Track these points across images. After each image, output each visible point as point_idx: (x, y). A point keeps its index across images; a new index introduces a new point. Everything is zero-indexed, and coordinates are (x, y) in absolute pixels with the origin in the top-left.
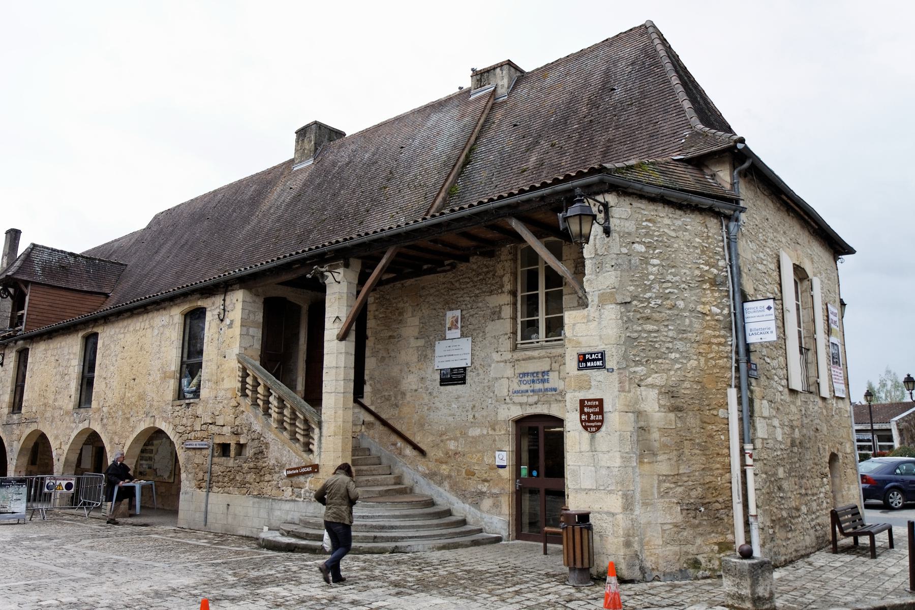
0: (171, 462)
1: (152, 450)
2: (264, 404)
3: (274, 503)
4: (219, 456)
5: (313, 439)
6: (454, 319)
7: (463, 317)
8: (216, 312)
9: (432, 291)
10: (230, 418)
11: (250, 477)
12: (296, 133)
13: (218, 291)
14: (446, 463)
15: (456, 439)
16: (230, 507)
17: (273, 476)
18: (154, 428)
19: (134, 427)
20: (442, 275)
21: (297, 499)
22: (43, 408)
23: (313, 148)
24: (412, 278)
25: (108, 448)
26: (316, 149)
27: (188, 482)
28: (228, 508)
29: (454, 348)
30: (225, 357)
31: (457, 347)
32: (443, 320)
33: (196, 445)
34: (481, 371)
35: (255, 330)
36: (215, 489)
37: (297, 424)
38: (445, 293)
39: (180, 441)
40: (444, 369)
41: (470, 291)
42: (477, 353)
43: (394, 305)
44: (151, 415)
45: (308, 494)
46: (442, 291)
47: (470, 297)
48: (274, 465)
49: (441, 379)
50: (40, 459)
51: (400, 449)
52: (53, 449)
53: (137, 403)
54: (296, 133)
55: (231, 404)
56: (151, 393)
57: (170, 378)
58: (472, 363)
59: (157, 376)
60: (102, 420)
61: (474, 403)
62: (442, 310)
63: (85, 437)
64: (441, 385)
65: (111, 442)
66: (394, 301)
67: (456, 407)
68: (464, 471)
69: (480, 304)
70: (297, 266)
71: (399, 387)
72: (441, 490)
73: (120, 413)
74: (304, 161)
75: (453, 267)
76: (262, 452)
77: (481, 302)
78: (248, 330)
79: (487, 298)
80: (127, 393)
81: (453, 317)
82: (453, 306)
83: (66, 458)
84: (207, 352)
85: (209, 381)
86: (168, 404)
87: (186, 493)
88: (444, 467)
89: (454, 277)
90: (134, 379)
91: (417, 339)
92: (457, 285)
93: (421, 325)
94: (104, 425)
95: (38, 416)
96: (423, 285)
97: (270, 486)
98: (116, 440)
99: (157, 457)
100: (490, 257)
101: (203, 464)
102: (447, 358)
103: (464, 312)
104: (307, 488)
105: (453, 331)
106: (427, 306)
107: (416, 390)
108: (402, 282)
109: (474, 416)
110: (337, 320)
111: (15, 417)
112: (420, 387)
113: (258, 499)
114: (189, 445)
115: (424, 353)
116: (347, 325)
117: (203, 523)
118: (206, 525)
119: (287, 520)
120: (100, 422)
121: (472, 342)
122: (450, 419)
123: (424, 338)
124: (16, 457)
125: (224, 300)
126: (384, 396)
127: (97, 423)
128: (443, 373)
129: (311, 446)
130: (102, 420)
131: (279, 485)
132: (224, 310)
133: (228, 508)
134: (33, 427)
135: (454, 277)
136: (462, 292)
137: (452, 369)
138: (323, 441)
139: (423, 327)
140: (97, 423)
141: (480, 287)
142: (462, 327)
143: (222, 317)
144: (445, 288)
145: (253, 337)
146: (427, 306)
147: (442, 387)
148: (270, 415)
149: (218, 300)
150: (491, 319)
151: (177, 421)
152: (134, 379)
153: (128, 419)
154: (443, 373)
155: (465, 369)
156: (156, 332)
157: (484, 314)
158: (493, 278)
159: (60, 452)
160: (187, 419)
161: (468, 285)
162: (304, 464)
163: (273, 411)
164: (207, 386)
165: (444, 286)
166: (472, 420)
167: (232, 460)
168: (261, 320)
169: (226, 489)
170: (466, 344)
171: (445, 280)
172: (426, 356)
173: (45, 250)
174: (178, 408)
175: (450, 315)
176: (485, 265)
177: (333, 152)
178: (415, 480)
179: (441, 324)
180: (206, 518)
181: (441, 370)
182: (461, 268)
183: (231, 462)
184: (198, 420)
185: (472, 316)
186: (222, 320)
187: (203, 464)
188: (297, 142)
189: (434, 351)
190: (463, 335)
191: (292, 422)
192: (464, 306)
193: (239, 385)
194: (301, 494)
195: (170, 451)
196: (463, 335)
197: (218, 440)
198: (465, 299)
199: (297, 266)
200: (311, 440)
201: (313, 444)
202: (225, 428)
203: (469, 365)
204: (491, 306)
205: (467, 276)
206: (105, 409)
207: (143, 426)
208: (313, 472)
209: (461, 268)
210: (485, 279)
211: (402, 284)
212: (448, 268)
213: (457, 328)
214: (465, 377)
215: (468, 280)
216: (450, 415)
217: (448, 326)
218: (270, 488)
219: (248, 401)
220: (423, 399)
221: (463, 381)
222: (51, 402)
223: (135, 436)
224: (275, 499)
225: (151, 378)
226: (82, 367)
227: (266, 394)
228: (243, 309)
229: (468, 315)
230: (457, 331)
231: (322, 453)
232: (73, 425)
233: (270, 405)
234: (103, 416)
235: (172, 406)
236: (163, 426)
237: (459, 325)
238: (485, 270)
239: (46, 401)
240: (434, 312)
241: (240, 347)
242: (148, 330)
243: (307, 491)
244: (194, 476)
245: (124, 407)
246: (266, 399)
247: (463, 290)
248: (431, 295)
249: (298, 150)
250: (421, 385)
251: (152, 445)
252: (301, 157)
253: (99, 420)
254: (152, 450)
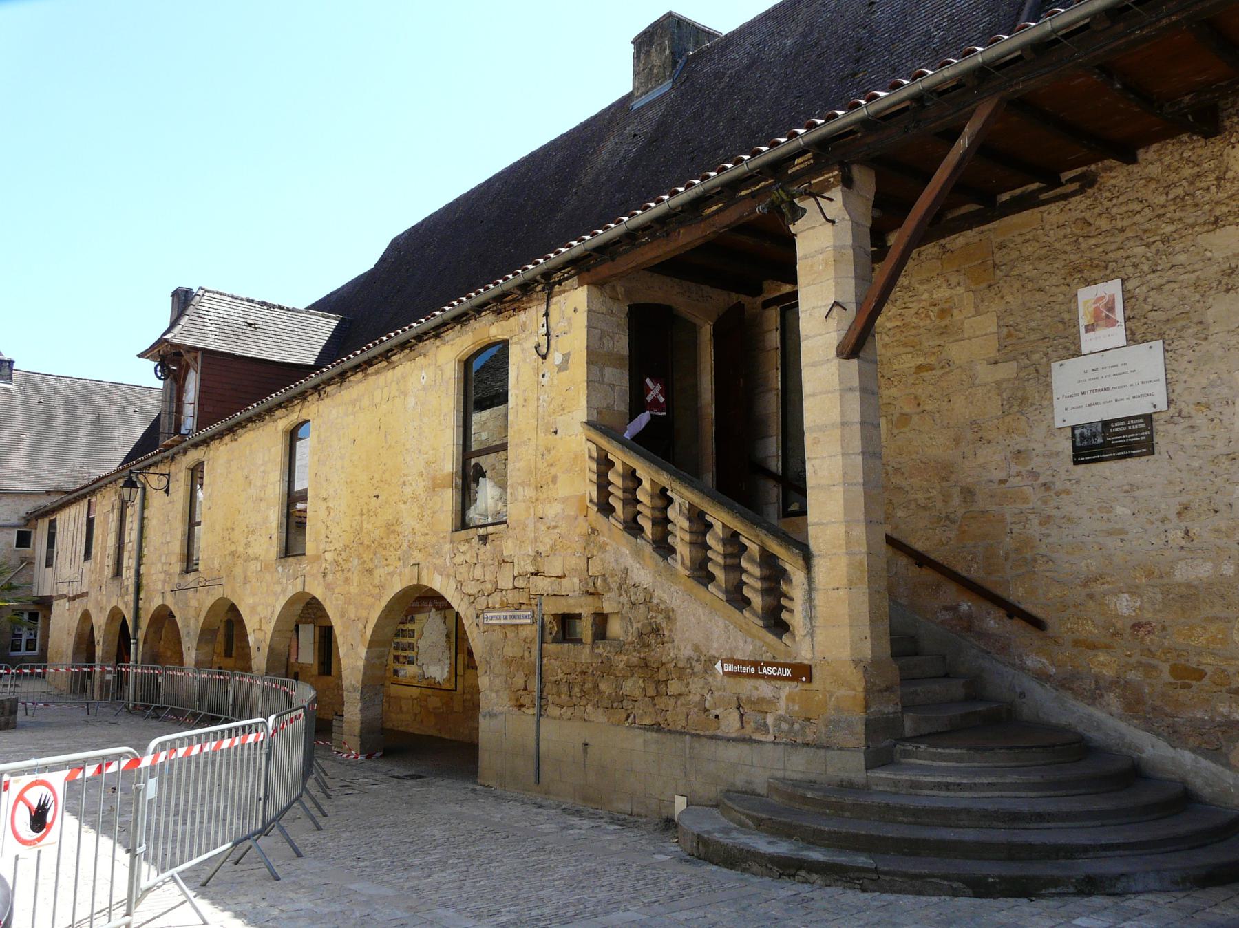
0: (447, 652)
1: (413, 631)
2: (654, 524)
3: (696, 745)
4: (555, 641)
5: (791, 599)
6: (1101, 305)
7: (1128, 297)
8: (533, 341)
9: (1029, 249)
10: (576, 562)
11: (632, 686)
12: (633, 42)
13: (531, 301)
14: (1108, 647)
15: (1133, 591)
16: (589, 749)
17: (688, 684)
18: (418, 587)
19: (381, 587)
20: (1054, 207)
21: (757, 736)
22: (229, 559)
23: (669, 63)
24: (970, 228)
25: (337, 630)
26: (675, 63)
27: (494, 695)
28: (585, 752)
29: (1108, 371)
30: (556, 432)
31: (1121, 369)
32: (1069, 311)
33: (505, 618)
34: (1199, 420)
35: (616, 371)
36: (553, 711)
37: (744, 564)
38: (1069, 248)
40: (1082, 426)
41: (1145, 231)
42: (1185, 377)
43: (926, 296)
44: (412, 562)
45: (785, 726)
46: (1057, 245)
47: (1148, 245)
48: (689, 659)
49: (1075, 448)
50: (237, 647)
51: (969, 617)
52: (249, 631)
53: (385, 541)
54: (633, 42)
56: (410, 521)
57: (444, 487)
58: (1170, 402)
59: (418, 486)
60: (325, 575)
61: (1184, 499)
62: (1063, 288)
63: (299, 608)
64: (1076, 463)
65: (342, 616)
66: (922, 288)
67: (1129, 512)
68: (1166, 668)
69: (1182, 258)
70: (715, 208)
71: (953, 477)
72: (1098, 713)
73: (356, 562)
74: (653, 88)
75: (1087, 182)
76: (657, 630)
77: (1185, 250)
78: (601, 371)
79: (1205, 239)
80: (365, 523)
81: (1099, 300)
82: (1096, 274)
83: (270, 646)
84: (516, 428)
85: (523, 484)
86: (444, 538)
87: (492, 715)
88: (1102, 659)
89: (1089, 208)
90: (377, 497)
91: (996, 363)
92: (1104, 223)
93: (1005, 331)
94: (329, 585)
95: (223, 574)
96: (1000, 239)
97: (683, 705)
98: (352, 611)
99: (422, 644)
100: (1207, 136)
101: (522, 657)
102: (1090, 398)
103: (1130, 285)
104: (782, 712)
105: (1101, 332)
106: (1017, 285)
107: (1003, 482)
108: (943, 242)
109: (1187, 532)
110: (836, 310)
111: (191, 577)
112: (1013, 472)
113: (654, 735)
114: (492, 618)
115: (1020, 394)
116: (859, 329)
117: (533, 779)
118: (538, 782)
119: (733, 785)
120: (321, 580)
121: (1165, 350)
122: (1112, 543)
123: (1014, 359)
124: (195, 644)
125: (547, 315)
126: (916, 500)
127: (316, 582)
128: (1082, 435)
129: (785, 616)
130: (325, 575)
131: (707, 705)
132: (548, 334)
133: (585, 752)
134: (218, 593)
135: (1089, 208)
136: (1121, 237)
137: (1106, 424)
138: (817, 602)
139: (1009, 335)
140: (316, 582)
141: (1178, 214)
142: (1127, 319)
143: (544, 351)
144: (1065, 237)
145: (612, 386)
146: (1017, 285)
147: (1081, 468)
148: (672, 550)
149: (532, 316)
150: (1223, 288)
152: (377, 497)
153: (370, 571)
154: (1082, 435)
155: (1148, 418)
156: (411, 401)
157: (1198, 278)
158: (1218, 187)
159: (260, 635)
160: (484, 566)
161: (1138, 218)
162: (767, 657)
163: (678, 539)
164: (520, 498)
165: (1061, 233)
166: (1183, 543)
167: (587, 650)
168: (626, 351)
169: (578, 712)
170: (1150, 357)
171: (1063, 218)
172: (1023, 401)
173: (223, 297)
174: (463, 548)
175: (1088, 297)
176: (1188, 160)
177: (711, 60)
178: (1018, 690)
179: (1062, 322)
180: (538, 768)
181: (1073, 428)
182: (1113, 182)
183: (584, 655)
184: (507, 567)
185: (1159, 288)
186: (544, 357)
187: (522, 657)
188: (637, 57)
189: (1048, 386)
190: (1132, 338)
191: (730, 561)
192: (1130, 270)
194: (766, 725)
195: (445, 632)
196: (1132, 338)
197: (551, 608)
198: (1130, 252)
199: (715, 208)
200: (783, 601)
201: (791, 611)
202: (565, 582)
203: (1163, 406)
204: (1218, 255)
205: (1133, 195)
206: (329, 556)
207: (397, 586)
208: (795, 678)
209: (1113, 182)
210: (1192, 195)
211: (943, 246)
212: (1076, 186)
213: (1112, 323)
214: (1151, 437)
215: (1137, 207)
216: (1109, 533)
217: (1083, 322)
218: (684, 709)
220: (1025, 500)
221: (1148, 448)
222: (241, 549)
223: (384, 603)
224: (698, 736)
225: (408, 491)
226: (287, 484)
227: (659, 503)
228: (589, 327)
229: (1144, 288)
230: (1111, 330)
231: (818, 631)
232: (278, 589)
233: (670, 527)
234: (326, 568)
236: (437, 583)
237: (1119, 315)
238: (1187, 172)
239: (233, 548)
240: (1039, 296)
241: (589, 407)
242: (397, 400)
243: (780, 719)
244: (506, 681)
245: (361, 549)
246: (657, 514)
247: (1122, 230)
248: (1026, 259)
249: (639, 74)
250: (1015, 469)
251: (412, 620)
252: (646, 83)
253: (321, 575)
254: (413, 631)
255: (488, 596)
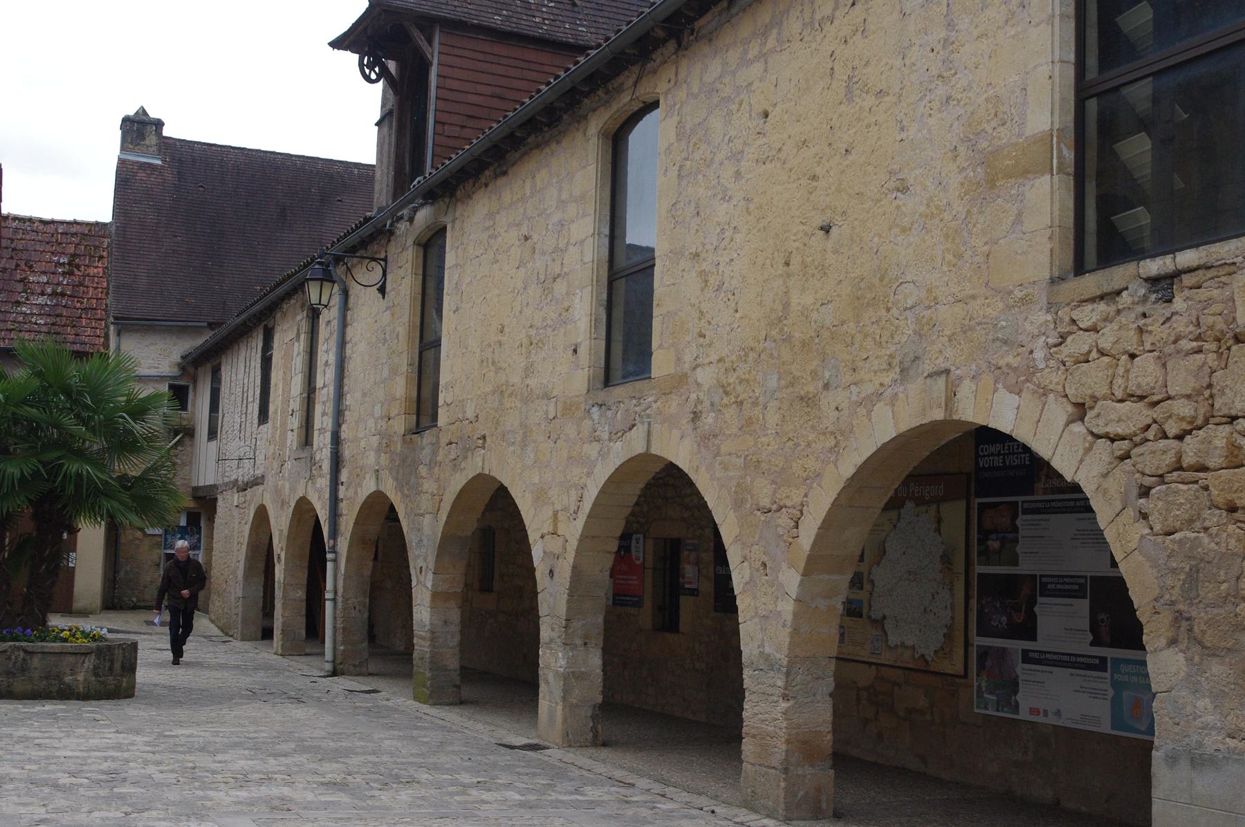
39: (1121, 479)
151: (1093, 378)
235: (1051, 306)
255: (1180, 437)
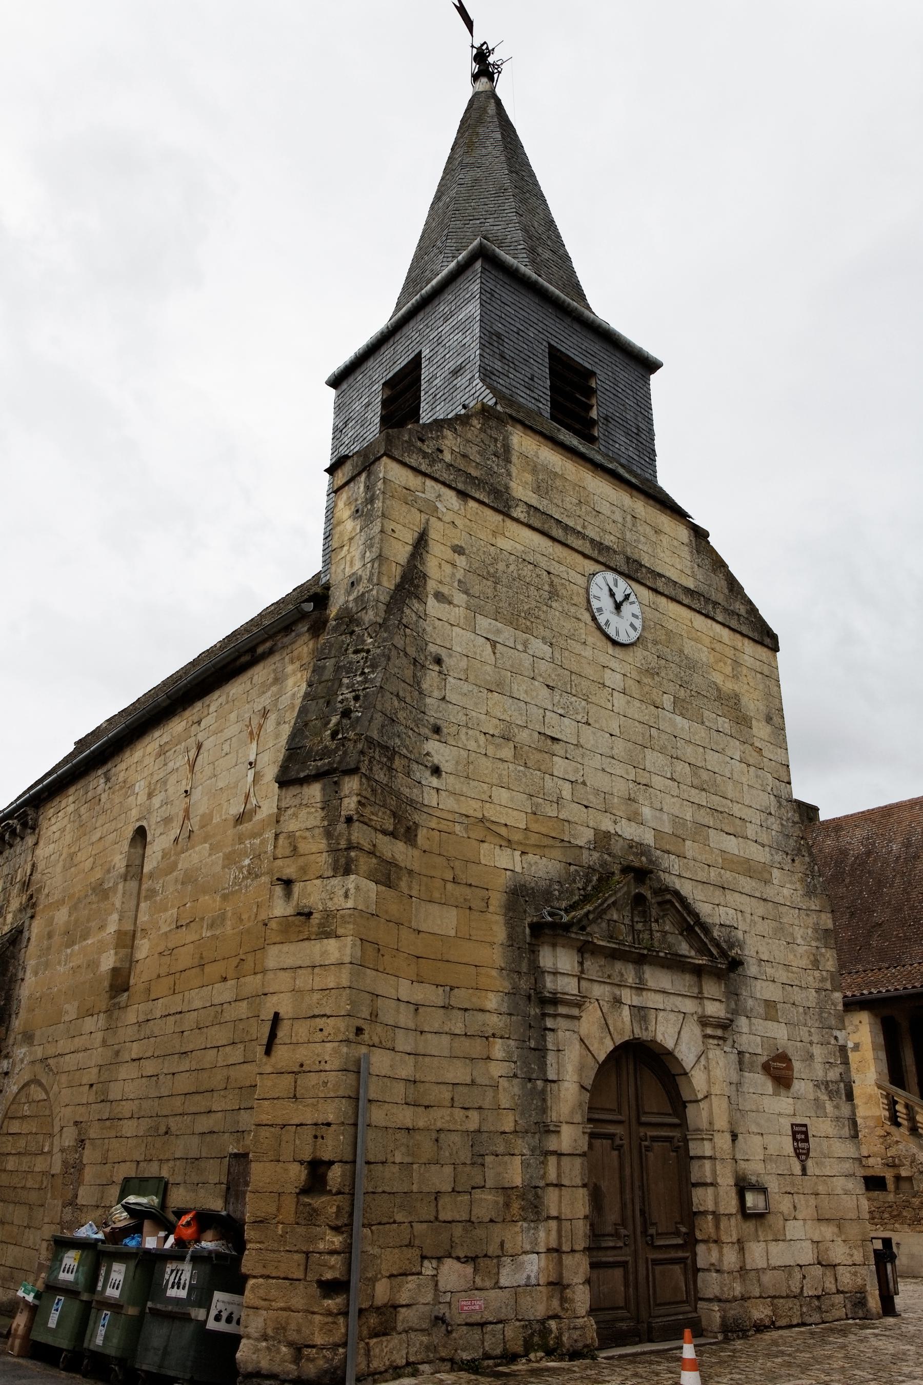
55: (877, 1134)
193: (887, 1114)
219: (904, 1130)
